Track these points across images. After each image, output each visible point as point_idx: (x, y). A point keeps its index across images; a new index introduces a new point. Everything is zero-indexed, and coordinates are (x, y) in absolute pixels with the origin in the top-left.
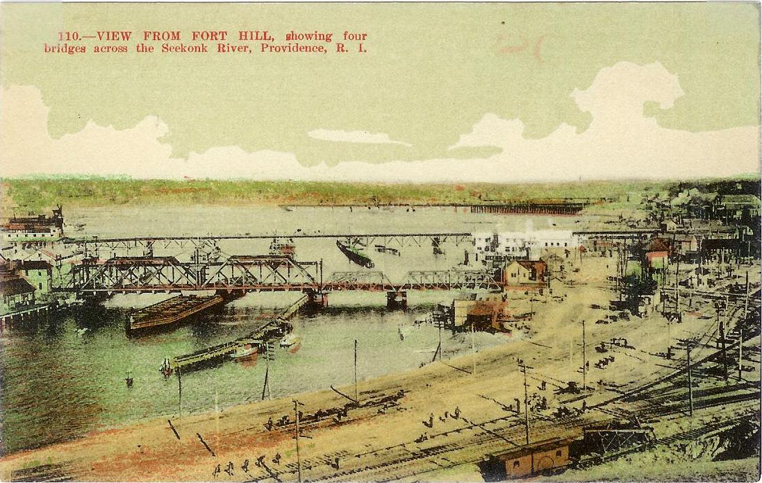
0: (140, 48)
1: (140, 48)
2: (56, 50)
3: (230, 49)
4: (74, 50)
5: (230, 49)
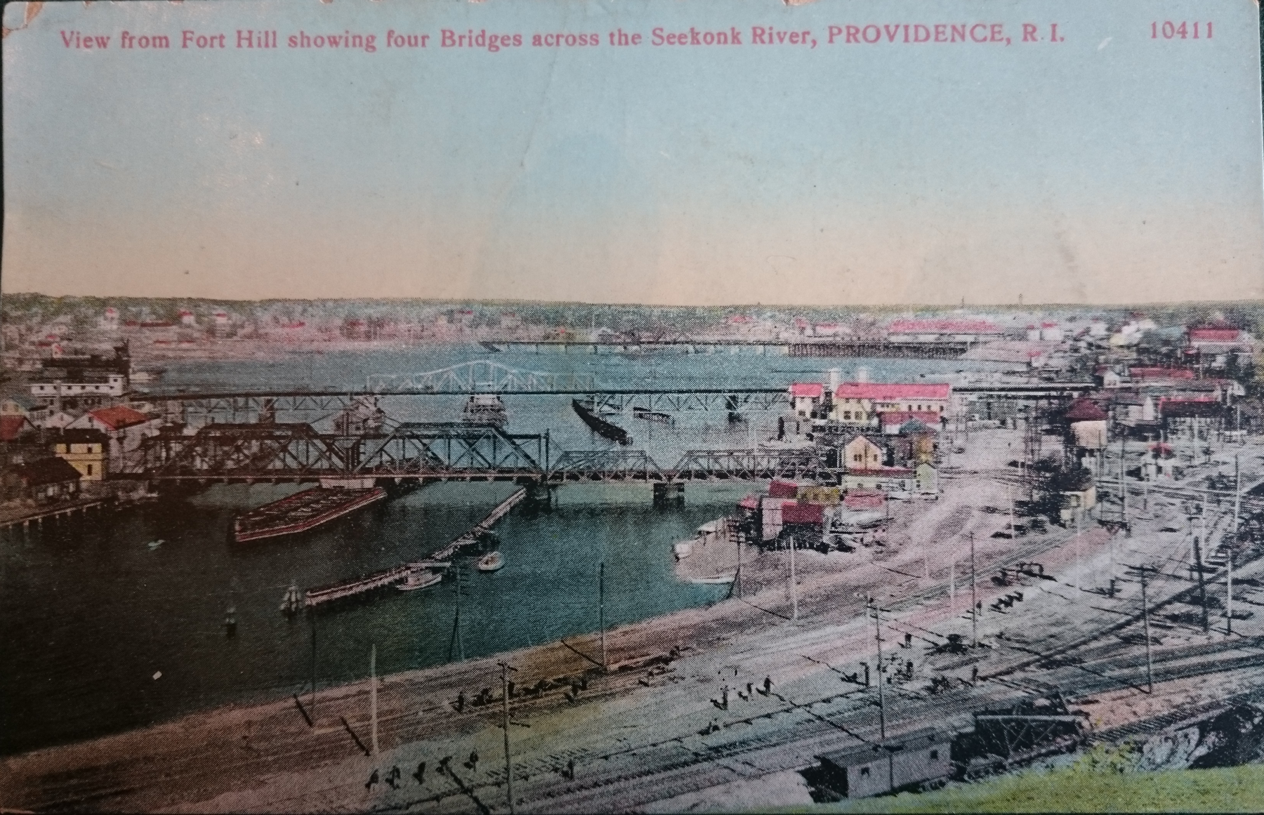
0: (616, 39)
1: (616, 39)
2: (465, 41)
3: (775, 37)
4: (498, 43)
5: (775, 37)
